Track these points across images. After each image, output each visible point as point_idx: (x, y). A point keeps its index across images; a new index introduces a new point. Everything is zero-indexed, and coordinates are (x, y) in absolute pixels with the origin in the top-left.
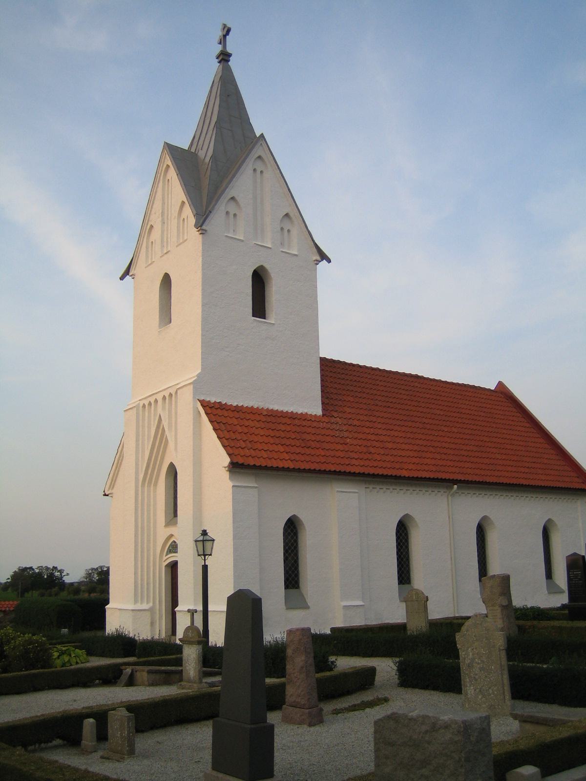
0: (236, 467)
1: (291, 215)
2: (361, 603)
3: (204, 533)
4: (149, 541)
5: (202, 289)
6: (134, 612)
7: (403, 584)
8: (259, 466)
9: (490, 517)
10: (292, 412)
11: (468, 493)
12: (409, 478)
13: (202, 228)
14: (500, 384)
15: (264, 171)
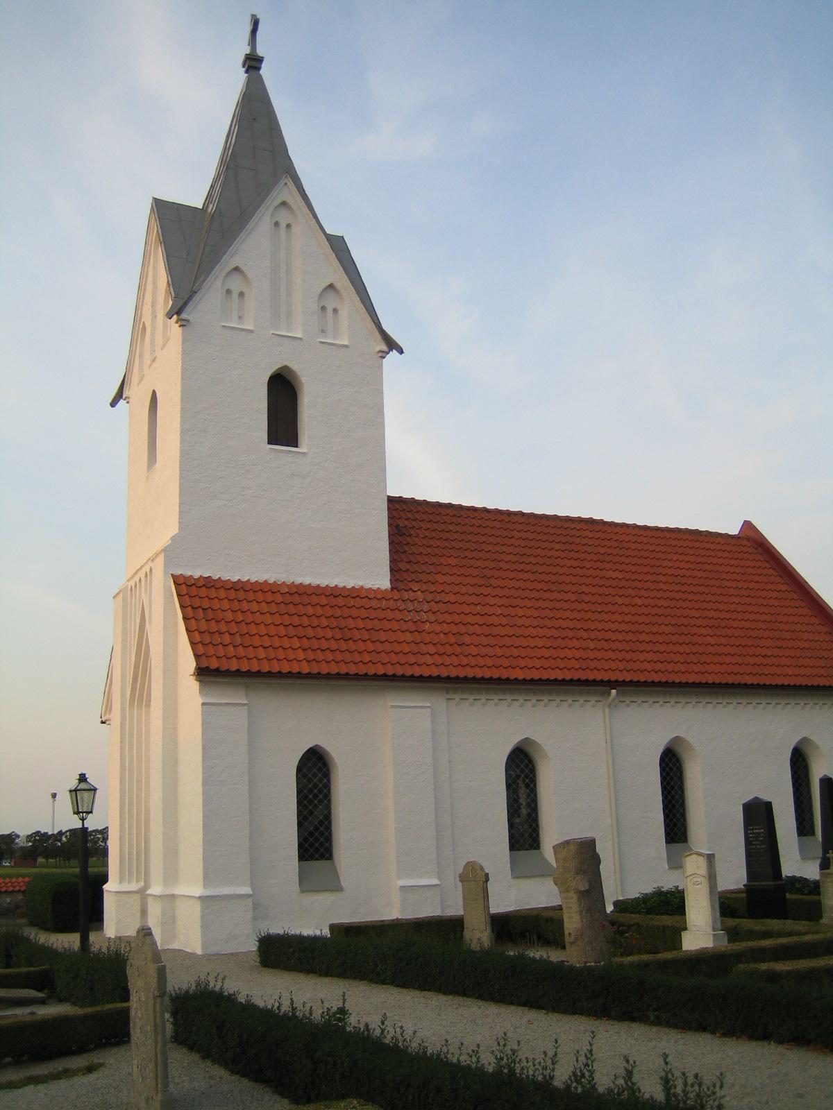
0: (203, 673)
1: (338, 285)
2: (435, 881)
3: (83, 778)
4: (139, 789)
5: (182, 409)
6: (119, 895)
7: (805, 835)
8: (246, 672)
9: (687, 739)
10: (336, 586)
11: (805, 704)
12: (525, 681)
13: (180, 317)
14: (747, 525)
15: (293, 224)
